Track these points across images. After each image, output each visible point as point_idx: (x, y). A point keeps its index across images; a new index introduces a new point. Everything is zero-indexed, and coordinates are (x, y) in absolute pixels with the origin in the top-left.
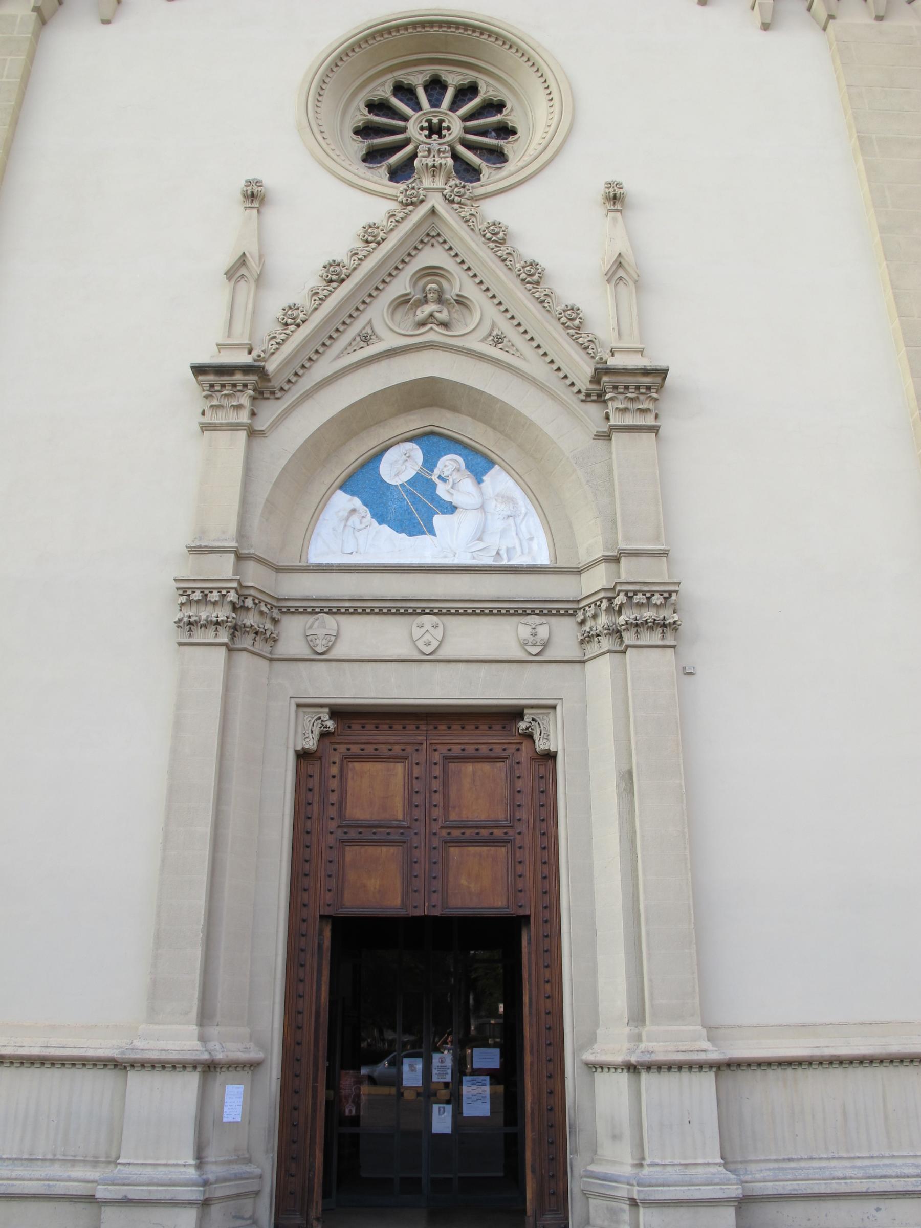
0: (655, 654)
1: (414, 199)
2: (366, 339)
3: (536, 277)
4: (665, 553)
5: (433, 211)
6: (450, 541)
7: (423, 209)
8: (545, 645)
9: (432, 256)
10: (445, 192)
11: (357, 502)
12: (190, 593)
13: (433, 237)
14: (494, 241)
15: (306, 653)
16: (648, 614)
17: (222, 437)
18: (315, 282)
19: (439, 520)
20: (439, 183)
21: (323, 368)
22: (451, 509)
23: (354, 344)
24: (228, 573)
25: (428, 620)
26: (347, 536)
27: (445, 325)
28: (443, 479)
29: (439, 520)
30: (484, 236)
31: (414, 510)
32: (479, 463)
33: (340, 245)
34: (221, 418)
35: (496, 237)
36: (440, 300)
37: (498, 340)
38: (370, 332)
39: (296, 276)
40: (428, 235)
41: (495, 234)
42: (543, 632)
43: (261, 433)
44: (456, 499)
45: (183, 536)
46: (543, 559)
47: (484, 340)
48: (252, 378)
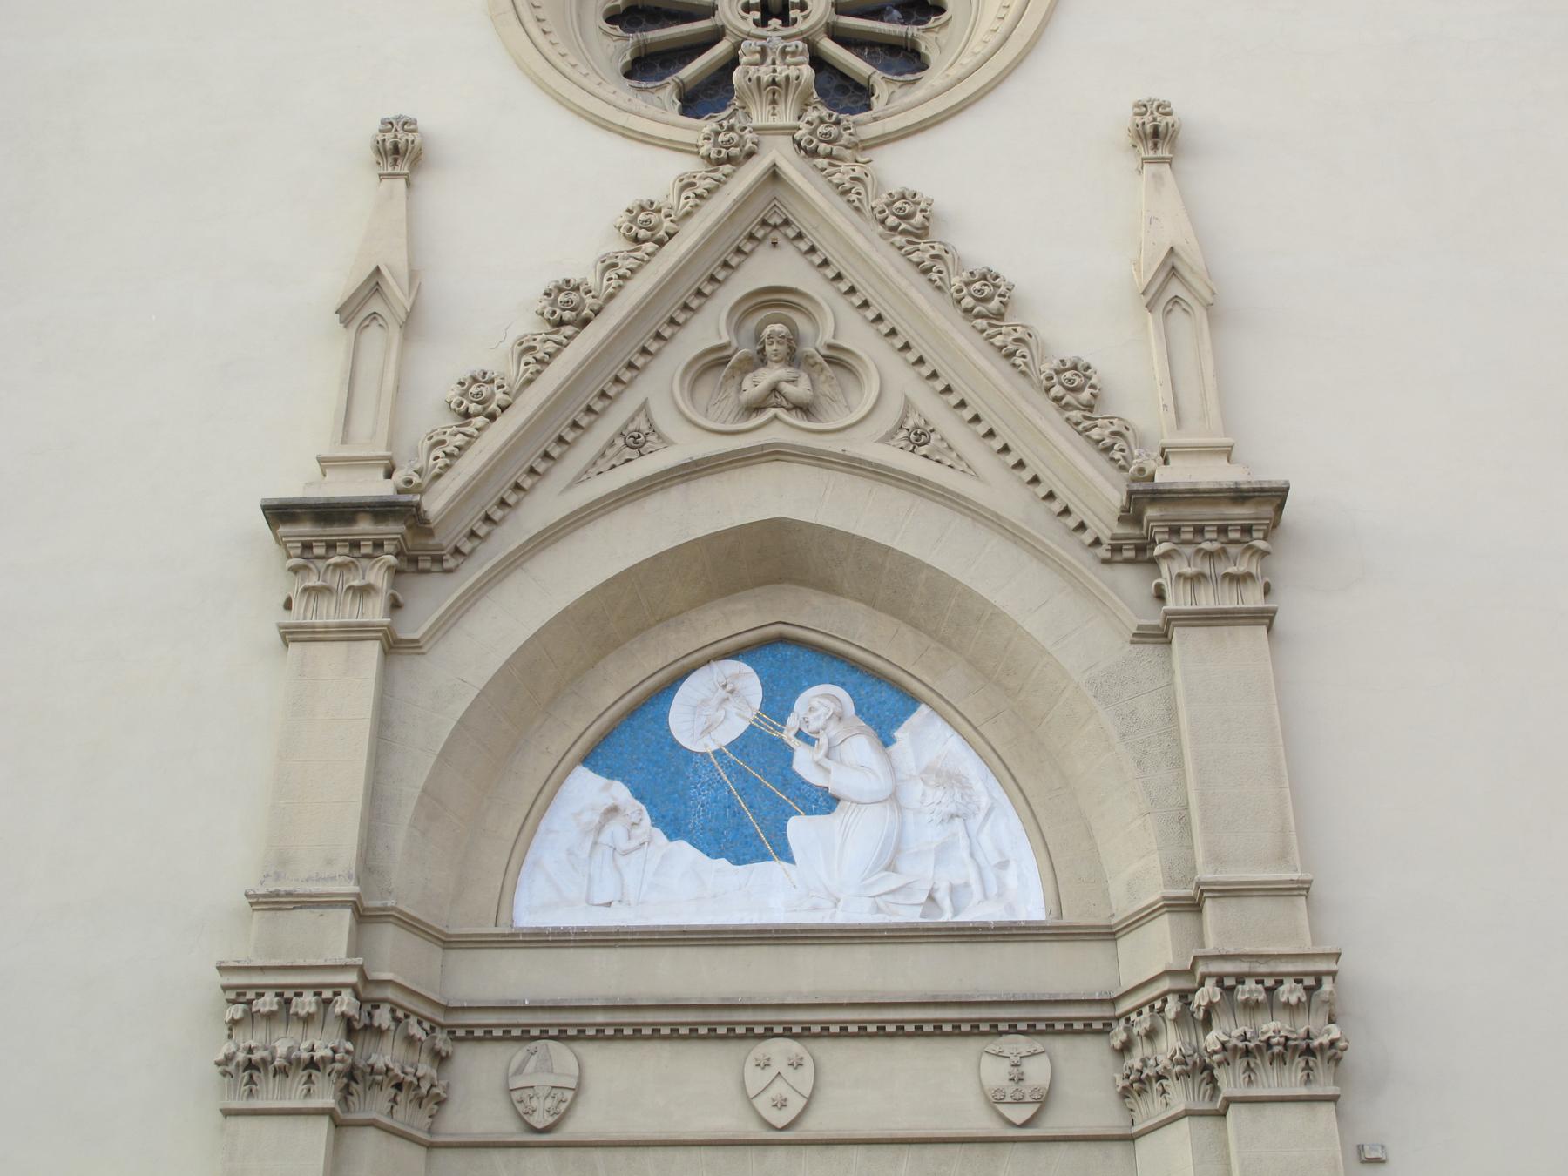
0: (1292, 1116)
1: (734, 151)
2: (636, 443)
3: (995, 304)
4: (1300, 889)
5: (774, 174)
6: (824, 873)
7: (752, 172)
8: (1043, 1102)
9: (775, 267)
10: (798, 135)
11: (620, 792)
12: (254, 998)
13: (775, 227)
14: (904, 232)
15: (508, 1128)
16: (1272, 1026)
17: (328, 655)
18: (527, 324)
19: (799, 828)
20: (786, 115)
21: (547, 504)
22: (825, 802)
23: (610, 453)
24: (340, 954)
25: (779, 1050)
26: (599, 867)
27: (804, 409)
28: (807, 739)
29: (799, 828)
30: (883, 222)
31: (747, 807)
32: (885, 702)
33: (580, 248)
34: (327, 613)
35: (909, 223)
36: (792, 357)
37: (919, 438)
38: (644, 427)
39: (486, 314)
40: (764, 223)
41: (907, 217)
42: (1037, 1072)
43: (413, 646)
44: (837, 781)
45: (242, 871)
46: (1032, 908)
47: (888, 438)
48: (393, 530)
